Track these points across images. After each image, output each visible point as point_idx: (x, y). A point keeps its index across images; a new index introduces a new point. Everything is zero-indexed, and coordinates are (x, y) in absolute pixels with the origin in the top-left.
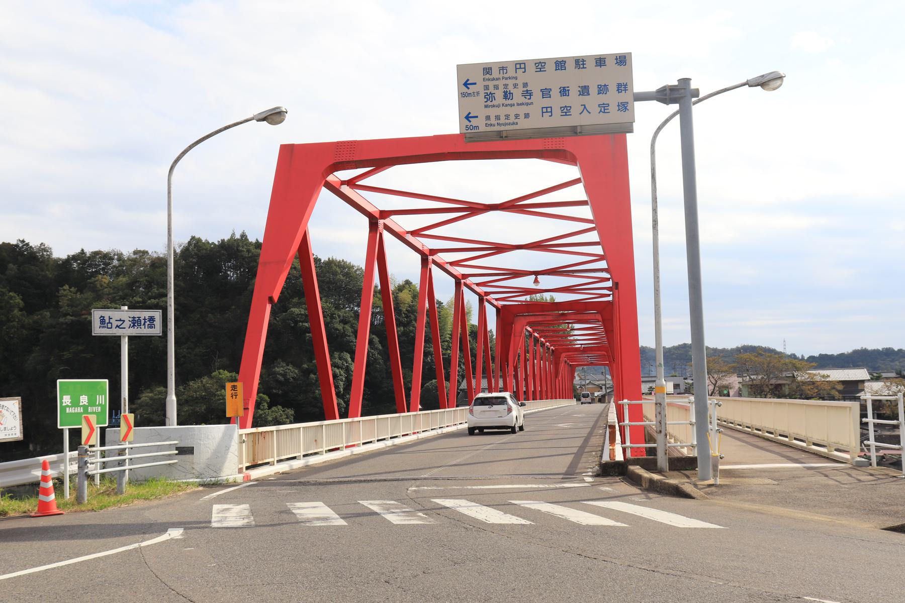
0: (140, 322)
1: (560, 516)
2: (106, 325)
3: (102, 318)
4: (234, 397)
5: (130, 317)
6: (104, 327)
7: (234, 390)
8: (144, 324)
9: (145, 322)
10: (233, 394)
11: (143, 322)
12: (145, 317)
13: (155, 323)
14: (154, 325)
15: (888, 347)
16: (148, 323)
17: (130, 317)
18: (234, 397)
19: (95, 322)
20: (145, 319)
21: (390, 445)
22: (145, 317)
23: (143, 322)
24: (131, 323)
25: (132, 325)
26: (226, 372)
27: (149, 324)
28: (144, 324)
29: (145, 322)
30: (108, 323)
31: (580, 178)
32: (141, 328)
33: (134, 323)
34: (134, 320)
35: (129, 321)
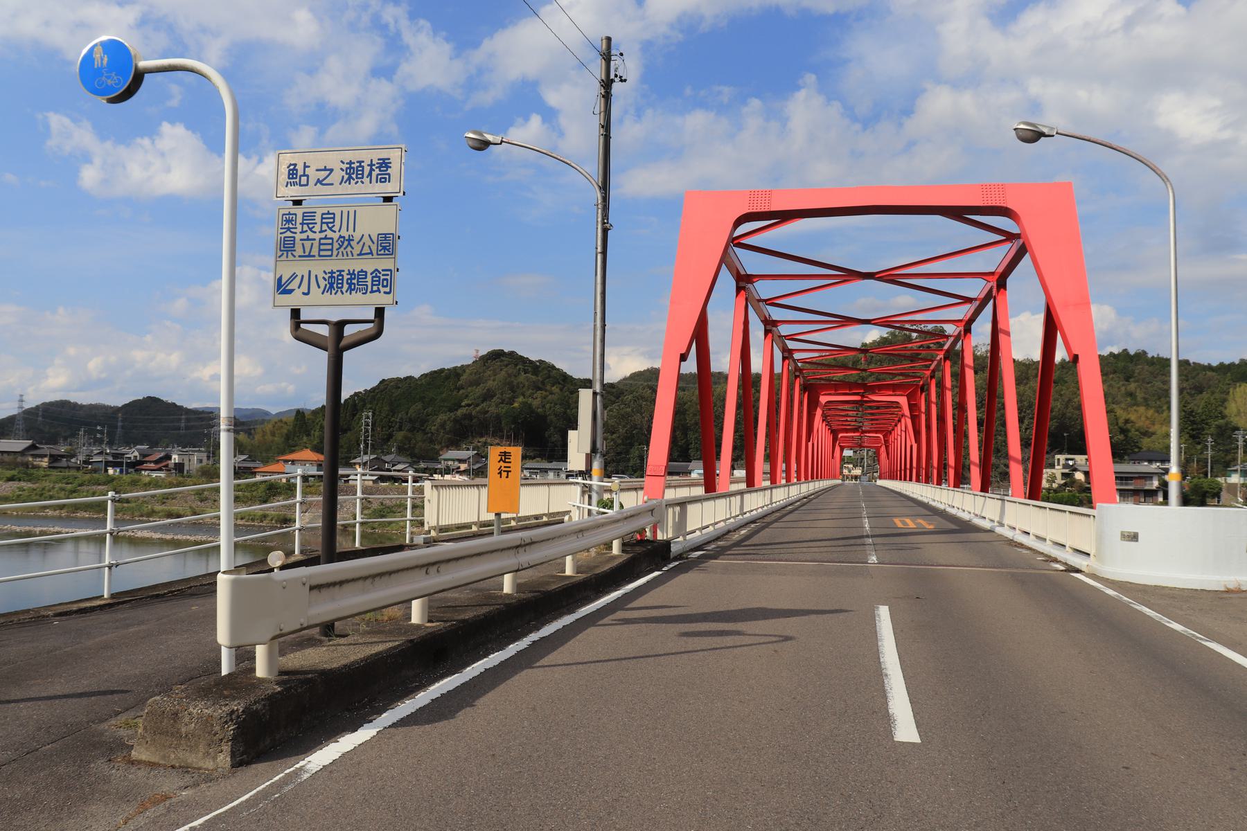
0: (363, 171)
2: (298, 180)
3: (292, 167)
4: (504, 474)
5: (343, 162)
7: (505, 462)
8: (370, 174)
9: (372, 170)
11: (367, 169)
13: (389, 171)
14: (389, 174)
16: (377, 171)
17: (343, 162)
18: (504, 474)
20: (371, 165)
23: (367, 169)
25: (346, 177)
27: (378, 175)
28: (370, 174)
29: (372, 170)
30: (301, 176)
33: (350, 174)
35: (342, 169)
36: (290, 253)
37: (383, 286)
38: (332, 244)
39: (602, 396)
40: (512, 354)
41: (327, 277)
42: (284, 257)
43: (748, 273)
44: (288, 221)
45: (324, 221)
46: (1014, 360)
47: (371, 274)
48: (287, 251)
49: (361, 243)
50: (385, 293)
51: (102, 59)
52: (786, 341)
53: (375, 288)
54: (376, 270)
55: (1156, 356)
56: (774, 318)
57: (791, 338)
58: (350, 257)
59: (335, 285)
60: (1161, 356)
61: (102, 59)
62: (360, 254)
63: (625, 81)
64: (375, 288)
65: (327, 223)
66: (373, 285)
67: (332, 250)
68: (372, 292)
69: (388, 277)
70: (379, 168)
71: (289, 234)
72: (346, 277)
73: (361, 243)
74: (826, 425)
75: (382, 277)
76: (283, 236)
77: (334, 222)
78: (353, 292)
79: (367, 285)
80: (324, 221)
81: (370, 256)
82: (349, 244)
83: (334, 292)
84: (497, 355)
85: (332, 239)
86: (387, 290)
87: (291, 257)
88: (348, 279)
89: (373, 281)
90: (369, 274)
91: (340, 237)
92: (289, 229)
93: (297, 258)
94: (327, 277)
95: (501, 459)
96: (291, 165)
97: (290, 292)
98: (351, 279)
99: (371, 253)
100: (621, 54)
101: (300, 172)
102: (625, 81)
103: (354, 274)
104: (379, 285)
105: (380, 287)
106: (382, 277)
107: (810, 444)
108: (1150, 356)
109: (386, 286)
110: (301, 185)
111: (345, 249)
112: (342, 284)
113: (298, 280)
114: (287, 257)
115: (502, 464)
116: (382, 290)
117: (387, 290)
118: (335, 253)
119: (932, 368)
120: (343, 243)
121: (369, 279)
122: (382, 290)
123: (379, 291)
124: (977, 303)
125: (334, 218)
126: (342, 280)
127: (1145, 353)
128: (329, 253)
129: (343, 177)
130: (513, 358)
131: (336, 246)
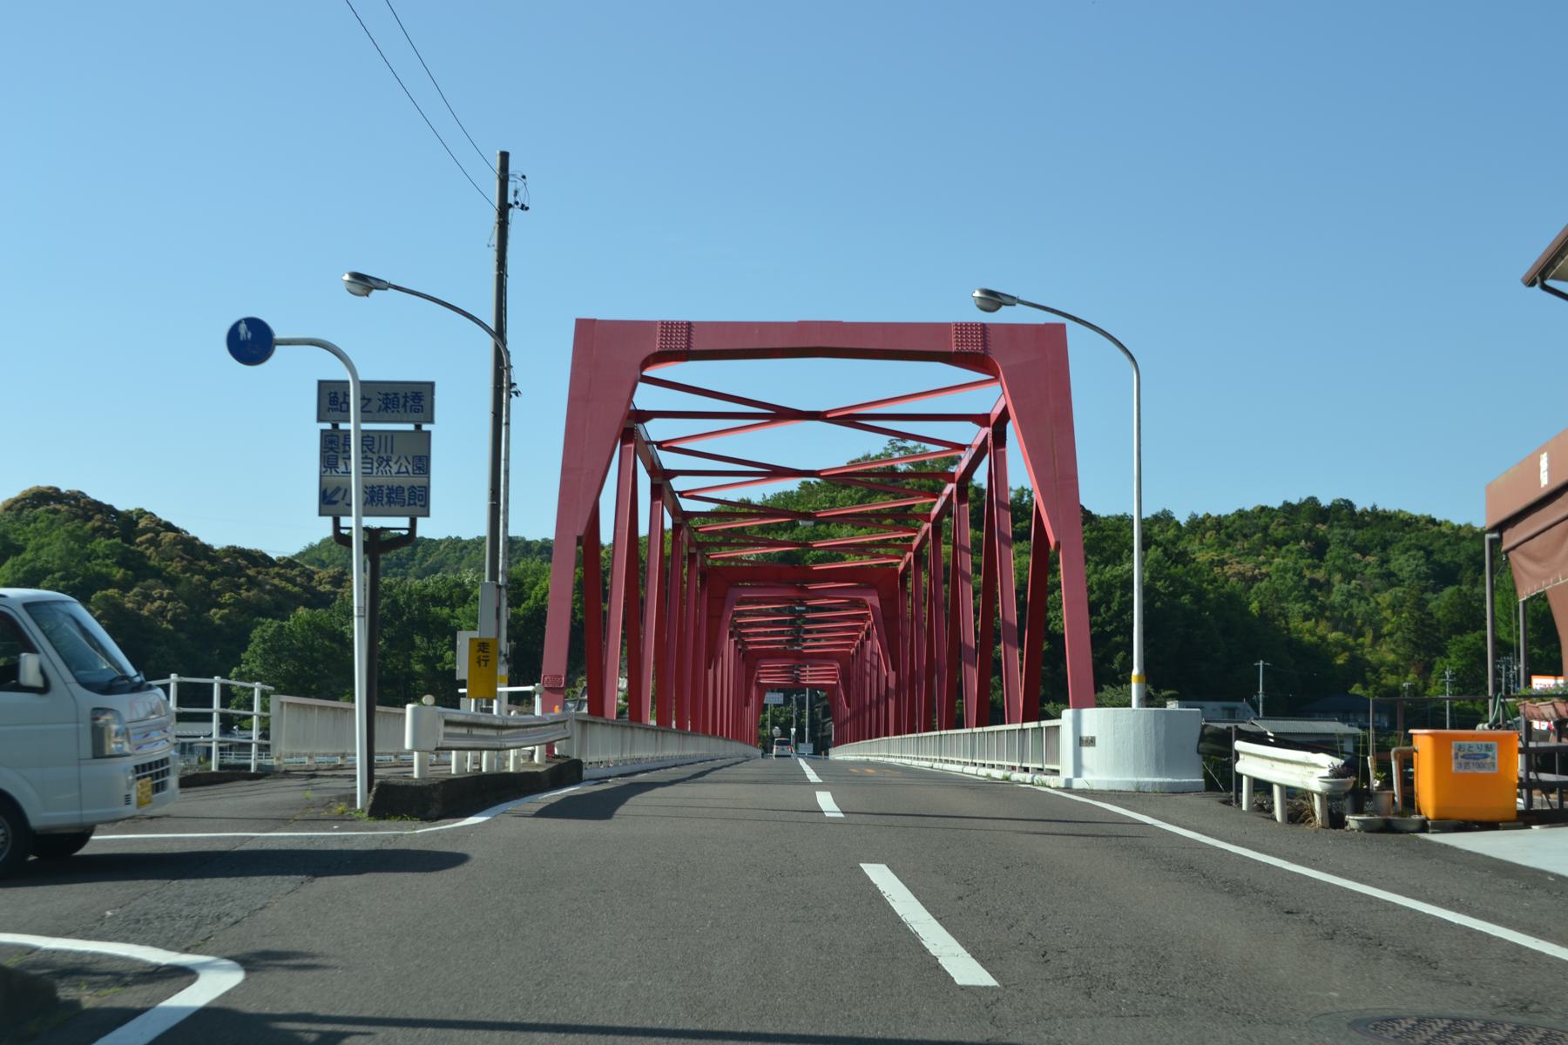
0: (398, 402)
1: (762, 584)
2: (339, 407)
3: (332, 395)
4: (483, 663)
5: (379, 393)
6: (336, 410)
7: (484, 652)
8: (405, 406)
9: (406, 401)
10: (482, 658)
11: (402, 401)
12: (406, 394)
13: (422, 403)
14: (422, 406)
15: (789, 490)
16: (411, 403)
17: (379, 393)
18: (483, 663)
19: (964, 592)
20: (406, 397)
21: (1000, 777)
22: (406, 394)
23: (402, 401)
24: (381, 403)
25: (383, 406)
26: (255, 631)
27: (412, 406)
28: (405, 406)
29: (406, 401)
30: (341, 403)
31: (485, 538)
32: (398, 411)
33: (386, 404)
34: (387, 398)
35: (380, 400)
36: (333, 470)
37: (419, 500)
38: (372, 463)
39: (508, 590)
40: (77, 498)
41: (368, 491)
42: (328, 473)
43: (638, 408)
44: (331, 442)
45: (365, 443)
46: (1088, 517)
47: (408, 489)
48: (331, 468)
49: (399, 464)
50: (421, 506)
51: (246, 334)
52: (680, 500)
53: (412, 502)
54: (413, 487)
55: (1369, 510)
56: (666, 466)
57: (691, 495)
58: (389, 474)
59: (376, 499)
60: (1380, 508)
61: (246, 334)
62: (398, 472)
63: (527, 208)
64: (412, 502)
65: (367, 445)
66: (409, 499)
67: (372, 468)
68: (409, 504)
69: (423, 493)
70: (413, 400)
71: (332, 453)
72: (385, 491)
73: (399, 464)
74: (736, 642)
75: (418, 493)
76: (326, 454)
77: (373, 444)
78: (392, 505)
79: (404, 499)
80: (365, 443)
81: (406, 475)
82: (388, 464)
83: (374, 504)
84: (43, 498)
85: (372, 459)
86: (422, 503)
87: (334, 472)
88: (387, 494)
89: (409, 495)
90: (406, 491)
91: (380, 457)
92: (332, 449)
93: (341, 474)
94: (368, 491)
95: (480, 650)
96: (331, 393)
97: (335, 503)
98: (390, 493)
99: (408, 472)
100: (524, 177)
101: (341, 400)
102: (527, 208)
103: (393, 489)
104: (415, 499)
105: (417, 501)
106: (418, 493)
107: (711, 672)
108: (1358, 509)
109: (421, 501)
110: (341, 411)
111: (384, 468)
112: (382, 497)
113: (341, 494)
114: (331, 472)
115: (481, 653)
116: (418, 503)
117: (422, 503)
118: (375, 470)
119: (916, 543)
120: (382, 462)
121: (406, 493)
122: (418, 503)
123: (415, 504)
124: (973, 450)
125: (373, 441)
126: (382, 494)
127: (1349, 505)
128: (369, 471)
129: (380, 407)
130: (82, 507)
131: (375, 465)
